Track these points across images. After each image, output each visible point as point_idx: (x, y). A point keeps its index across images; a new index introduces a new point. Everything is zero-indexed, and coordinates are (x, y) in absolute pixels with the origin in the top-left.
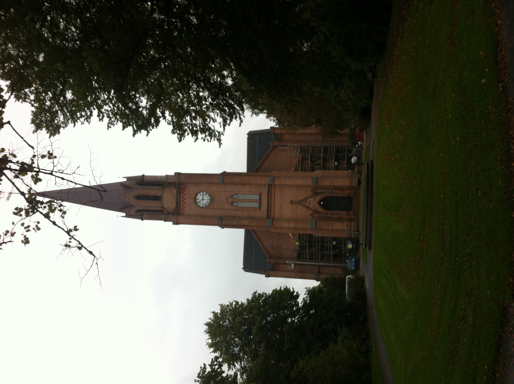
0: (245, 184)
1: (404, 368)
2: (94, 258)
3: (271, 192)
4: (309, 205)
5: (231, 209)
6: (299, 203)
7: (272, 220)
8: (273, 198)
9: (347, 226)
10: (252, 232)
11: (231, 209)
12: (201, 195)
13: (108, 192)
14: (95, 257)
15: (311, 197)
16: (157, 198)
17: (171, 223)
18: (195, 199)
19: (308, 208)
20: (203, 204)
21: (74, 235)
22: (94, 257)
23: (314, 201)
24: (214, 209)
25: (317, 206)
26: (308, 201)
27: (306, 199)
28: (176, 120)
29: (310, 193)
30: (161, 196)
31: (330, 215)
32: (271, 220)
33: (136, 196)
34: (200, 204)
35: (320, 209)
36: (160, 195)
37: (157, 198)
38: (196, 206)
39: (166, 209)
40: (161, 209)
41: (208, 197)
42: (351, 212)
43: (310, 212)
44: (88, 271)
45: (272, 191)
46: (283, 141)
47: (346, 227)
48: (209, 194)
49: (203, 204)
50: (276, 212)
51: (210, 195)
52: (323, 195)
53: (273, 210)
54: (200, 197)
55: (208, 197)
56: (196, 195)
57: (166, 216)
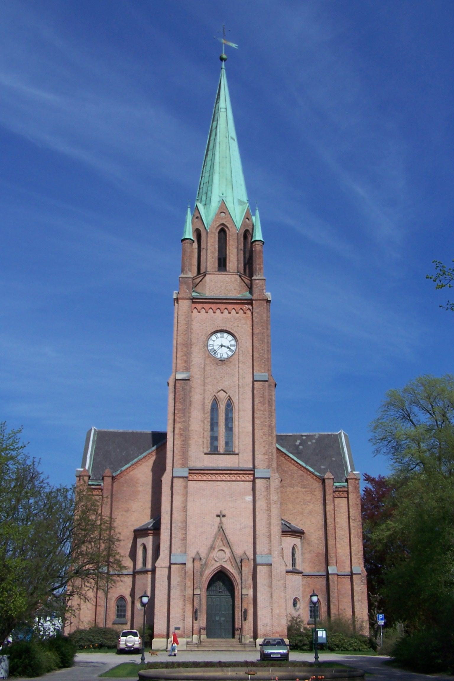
0: (239, 366)
4: (216, 550)
5: (204, 398)
7: (186, 477)
11: (204, 398)
12: (231, 345)
13: (287, 572)
16: (222, 264)
20: (213, 345)
23: (224, 560)
24: (205, 365)
25: (216, 566)
26: (223, 548)
28: (340, 431)
30: (225, 270)
31: (199, 593)
32: (186, 474)
33: (226, 229)
37: (222, 264)
38: (210, 333)
39: (203, 280)
41: (227, 354)
42: (203, 637)
46: (334, 497)
48: (231, 356)
49: (213, 345)
51: (230, 357)
52: (239, 581)
53: (205, 478)
54: (227, 339)
55: (227, 354)
57: (190, 279)
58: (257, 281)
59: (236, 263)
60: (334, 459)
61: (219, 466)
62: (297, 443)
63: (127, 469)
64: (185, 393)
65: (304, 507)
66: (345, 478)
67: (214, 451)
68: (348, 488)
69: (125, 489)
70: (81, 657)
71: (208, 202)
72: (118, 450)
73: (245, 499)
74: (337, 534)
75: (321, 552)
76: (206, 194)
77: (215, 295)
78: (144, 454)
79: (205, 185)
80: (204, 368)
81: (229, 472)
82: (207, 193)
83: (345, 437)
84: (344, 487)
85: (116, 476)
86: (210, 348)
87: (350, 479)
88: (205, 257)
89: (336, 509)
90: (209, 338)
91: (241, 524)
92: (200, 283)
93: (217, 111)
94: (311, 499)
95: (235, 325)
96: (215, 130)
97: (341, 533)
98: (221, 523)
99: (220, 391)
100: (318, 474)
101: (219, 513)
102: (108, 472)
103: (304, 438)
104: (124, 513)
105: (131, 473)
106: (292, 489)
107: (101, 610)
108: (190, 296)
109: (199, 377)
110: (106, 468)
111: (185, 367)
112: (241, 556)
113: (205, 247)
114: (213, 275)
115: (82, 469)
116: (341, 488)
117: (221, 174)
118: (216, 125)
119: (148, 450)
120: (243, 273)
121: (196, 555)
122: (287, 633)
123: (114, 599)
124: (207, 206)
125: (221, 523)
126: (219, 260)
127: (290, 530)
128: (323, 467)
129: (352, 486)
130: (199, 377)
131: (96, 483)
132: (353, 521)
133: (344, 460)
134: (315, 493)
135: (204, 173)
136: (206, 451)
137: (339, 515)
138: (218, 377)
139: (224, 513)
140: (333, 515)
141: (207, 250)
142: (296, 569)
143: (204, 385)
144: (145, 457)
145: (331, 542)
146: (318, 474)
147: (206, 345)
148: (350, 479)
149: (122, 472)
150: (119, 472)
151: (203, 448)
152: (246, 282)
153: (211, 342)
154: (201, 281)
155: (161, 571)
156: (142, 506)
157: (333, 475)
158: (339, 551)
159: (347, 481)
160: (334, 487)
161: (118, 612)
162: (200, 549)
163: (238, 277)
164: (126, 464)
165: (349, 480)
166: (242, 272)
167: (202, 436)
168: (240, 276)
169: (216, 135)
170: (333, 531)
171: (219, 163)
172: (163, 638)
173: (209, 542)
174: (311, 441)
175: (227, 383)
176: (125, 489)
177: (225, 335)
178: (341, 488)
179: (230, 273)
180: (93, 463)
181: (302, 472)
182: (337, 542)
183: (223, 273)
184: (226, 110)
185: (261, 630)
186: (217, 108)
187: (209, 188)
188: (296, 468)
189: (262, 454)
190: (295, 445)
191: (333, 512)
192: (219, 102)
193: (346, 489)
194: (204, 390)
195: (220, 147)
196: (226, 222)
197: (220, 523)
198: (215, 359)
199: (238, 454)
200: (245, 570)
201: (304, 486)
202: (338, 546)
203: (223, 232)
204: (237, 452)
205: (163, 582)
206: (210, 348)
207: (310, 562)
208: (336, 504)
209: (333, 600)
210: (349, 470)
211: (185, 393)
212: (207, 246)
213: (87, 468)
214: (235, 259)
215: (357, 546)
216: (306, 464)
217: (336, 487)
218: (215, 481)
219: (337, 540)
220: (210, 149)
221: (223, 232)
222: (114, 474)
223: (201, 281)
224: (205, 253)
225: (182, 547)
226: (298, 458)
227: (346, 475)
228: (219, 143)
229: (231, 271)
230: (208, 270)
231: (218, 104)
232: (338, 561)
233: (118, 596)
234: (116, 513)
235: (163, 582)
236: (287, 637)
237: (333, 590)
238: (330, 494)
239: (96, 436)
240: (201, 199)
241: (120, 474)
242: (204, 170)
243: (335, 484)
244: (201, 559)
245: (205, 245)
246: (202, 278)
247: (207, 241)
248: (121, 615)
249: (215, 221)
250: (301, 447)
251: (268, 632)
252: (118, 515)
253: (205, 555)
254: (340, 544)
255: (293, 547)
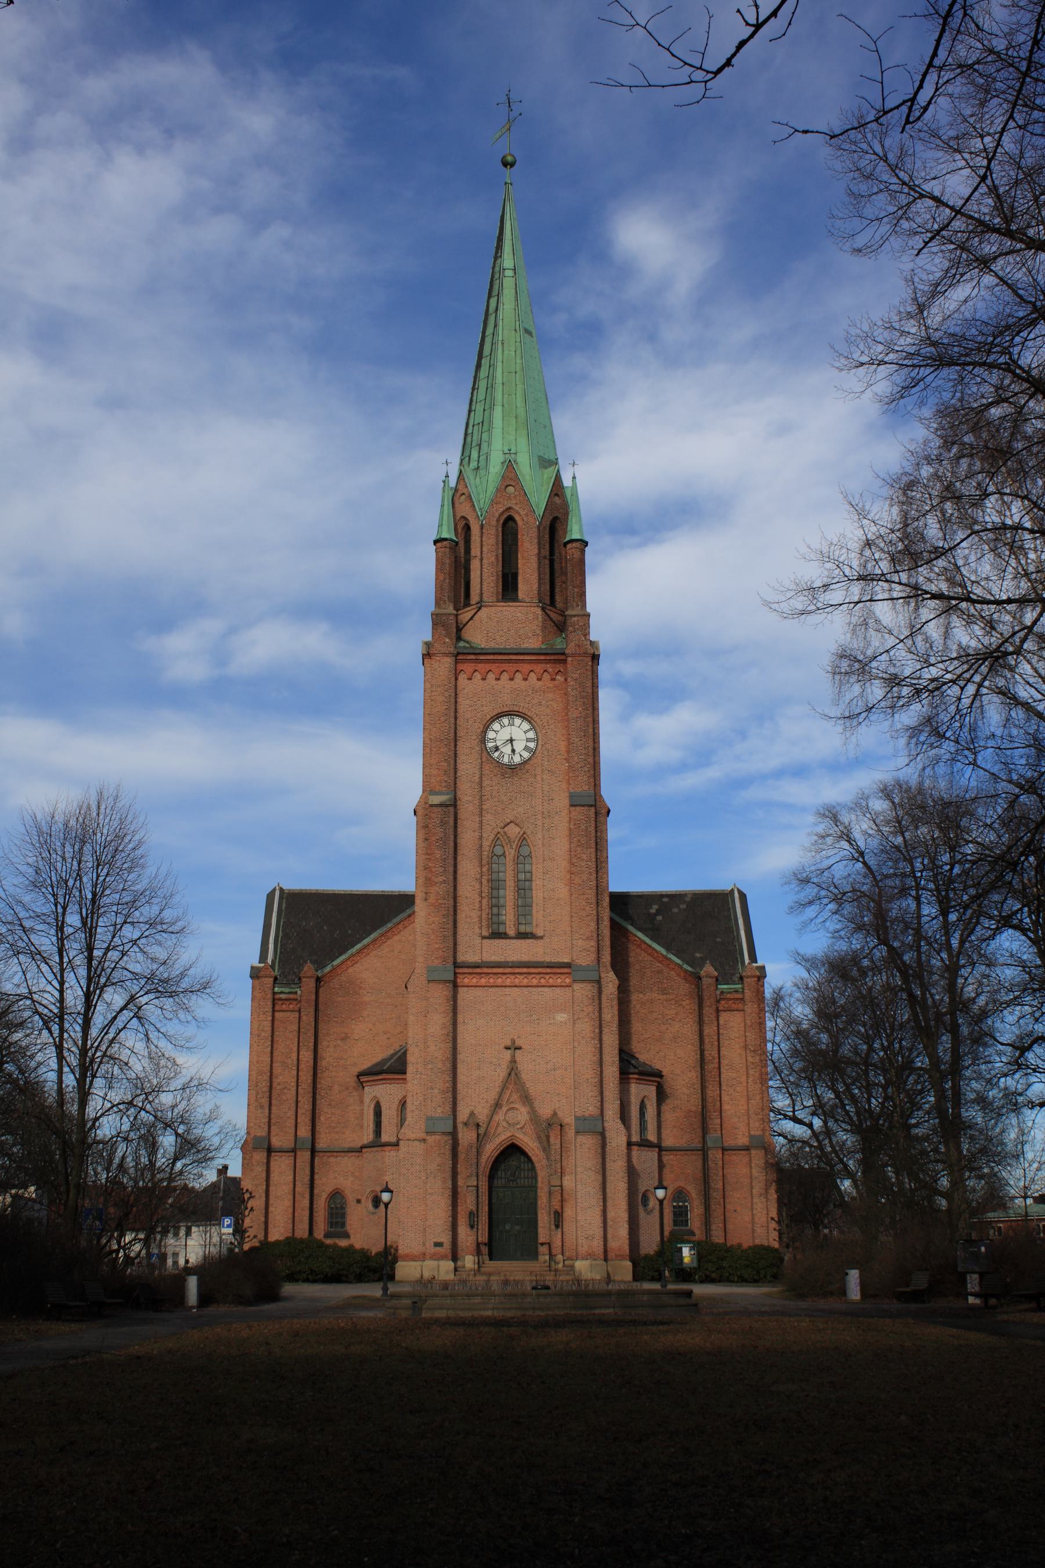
1: (80, 1361)
2: (712, 73)
3: (547, 973)
5: (481, 838)
6: (513, 1071)
8: (525, 982)
9: (438, 1244)
10: (409, 912)
11: (481, 838)
14: (713, 75)
15: (534, 1117)
16: (509, 587)
17: (429, 638)
18: (510, 714)
19: (497, 1105)
21: (747, 24)
22: (714, 70)
23: (518, 1126)
24: (481, 778)
27: (527, 1099)
29: (545, 1111)
30: (515, 599)
34: (496, 732)
35: (491, 1149)
36: (521, 595)
37: (509, 587)
38: (489, 717)
40: (474, 598)
43: (482, 1114)
44: (668, 50)
45: (547, 977)
47: (435, 1240)
48: (529, 759)
49: (495, 740)
50: (478, 992)
51: (525, 762)
56: (524, 717)
58: (575, 619)
59: (536, 585)
60: (719, 940)
61: (508, 960)
62: (653, 911)
63: (343, 963)
64: (445, 830)
65: (663, 1028)
66: (738, 975)
67: (498, 935)
68: (743, 992)
69: (340, 999)
70: (289, 1289)
71: (482, 463)
72: (325, 928)
73: (554, 1019)
74: (723, 1076)
75: (694, 1109)
76: (477, 448)
77: (497, 646)
78: (372, 936)
79: (476, 427)
80: (481, 783)
81: (525, 970)
82: (480, 445)
83: (740, 898)
84: (737, 991)
85: (323, 976)
86: (490, 745)
87: (748, 977)
88: (479, 572)
89: (721, 1031)
90: (488, 727)
91: (547, 1063)
92: (470, 623)
93: (497, 276)
94: (676, 1014)
95: (535, 701)
96: (494, 315)
97: (730, 1074)
98: (513, 1061)
99: (509, 824)
100: (690, 969)
101: (509, 1043)
102: (308, 969)
103: (665, 900)
104: (339, 1042)
105: (350, 970)
106: (641, 995)
107: (303, 1215)
108: (452, 650)
109: (471, 798)
110: (305, 962)
111: (446, 781)
112: (547, 1120)
113: (479, 554)
114: (493, 608)
115: (263, 965)
116: (729, 993)
117: (506, 406)
118: (495, 305)
119: (379, 928)
120: (548, 602)
121: (469, 1118)
122: (628, 1251)
123: (324, 1196)
124: (482, 472)
125: (513, 1061)
126: (505, 576)
127: (637, 1071)
128: (698, 955)
129: (750, 990)
130: (471, 798)
131: (287, 990)
132: (752, 1054)
133: (738, 940)
134: (684, 1003)
135: (474, 403)
136: (485, 933)
137: (727, 1043)
138: (504, 798)
139: (517, 1044)
140: (716, 1043)
141: (482, 559)
142: (647, 1140)
143: (481, 815)
144: (375, 940)
145: (712, 1091)
146: (690, 969)
147: (483, 740)
148: (748, 977)
149: (334, 969)
150: (328, 968)
151: (481, 928)
152: (554, 619)
153: (491, 735)
154: (471, 619)
155: (409, 1146)
156: (371, 1030)
157: (716, 970)
158: (725, 1107)
159: (741, 978)
160: (718, 992)
161: (332, 1217)
162: (475, 1107)
163: (539, 611)
164: (341, 954)
165: (745, 979)
166: (547, 600)
167: (478, 905)
168: (543, 609)
169: (495, 326)
170: (715, 1072)
171: (503, 384)
172: (414, 1260)
173: (492, 1096)
174: (678, 907)
175: (521, 809)
176: (340, 999)
177: (517, 721)
178: (729, 993)
179: (525, 604)
180: (281, 953)
181: (659, 965)
182: (723, 1092)
183: (510, 604)
184: (515, 273)
185: (582, 1247)
186: (497, 269)
187: (485, 436)
188: (650, 958)
189: (584, 938)
190: (649, 914)
191: (716, 1038)
192: (501, 256)
193: (740, 996)
194: (481, 822)
195: (503, 351)
196: (516, 504)
197: (511, 1062)
198: (498, 764)
199: (541, 938)
200: (555, 1144)
201: (664, 991)
202: (725, 1098)
203: (508, 527)
204: (540, 933)
205: (412, 1164)
206: (490, 745)
207: (674, 1127)
208: (721, 1022)
209: (715, 1194)
210: (747, 960)
211: (445, 830)
212: (482, 552)
213: (269, 961)
214: (533, 577)
215: (758, 1097)
216: (668, 949)
217: (722, 993)
218: (501, 986)
219: (724, 1087)
220: (484, 355)
221: (508, 527)
222: (319, 974)
223: (471, 619)
224: (479, 567)
225: (443, 1103)
226: (652, 939)
227: (740, 970)
228: (503, 344)
229: (527, 600)
230: (485, 599)
231: (498, 261)
232: (724, 1125)
233: (331, 1190)
234: (325, 1043)
235: (412, 1164)
236: (628, 1258)
237: (715, 1177)
238: (710, 1006)
239: (284, 901)
240: (470, 457)
241: (331, 971)
242: (475, 398)
243: (719, 987)
244: (478, 1125)
245: (479, 549)
246: (473, 612)
247: (482, 541)
248: (337, 1223)
249: (494, 502)
250: (659, 918)
251: (595, 1250)
252: (328, 1046)
253: (484, 1118)
254: (728, 1095)
255: (643, 1101)
